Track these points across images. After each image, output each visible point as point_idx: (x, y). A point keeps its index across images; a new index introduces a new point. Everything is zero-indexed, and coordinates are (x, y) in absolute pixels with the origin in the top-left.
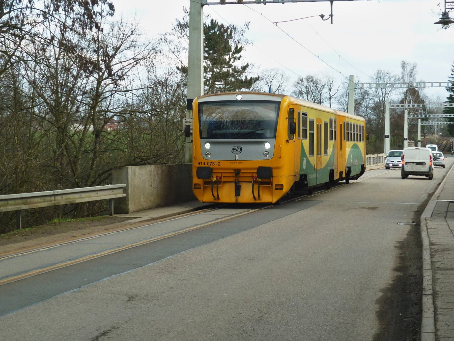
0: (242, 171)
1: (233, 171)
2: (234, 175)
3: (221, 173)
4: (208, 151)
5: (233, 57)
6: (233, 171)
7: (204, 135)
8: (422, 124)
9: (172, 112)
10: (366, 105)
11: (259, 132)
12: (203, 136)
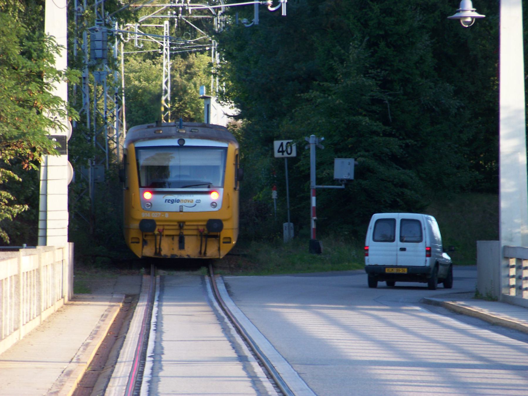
0: (187, 224)
1: (176, 224)
2: (177, 227)
3: (164, 225)
4: (148, 201)
5: (103, 58)
6: (176, 224)
7: (143, 184)
9: (40, 136)
10: (160, 50)
11: (121, 156)
12: (376, 238)
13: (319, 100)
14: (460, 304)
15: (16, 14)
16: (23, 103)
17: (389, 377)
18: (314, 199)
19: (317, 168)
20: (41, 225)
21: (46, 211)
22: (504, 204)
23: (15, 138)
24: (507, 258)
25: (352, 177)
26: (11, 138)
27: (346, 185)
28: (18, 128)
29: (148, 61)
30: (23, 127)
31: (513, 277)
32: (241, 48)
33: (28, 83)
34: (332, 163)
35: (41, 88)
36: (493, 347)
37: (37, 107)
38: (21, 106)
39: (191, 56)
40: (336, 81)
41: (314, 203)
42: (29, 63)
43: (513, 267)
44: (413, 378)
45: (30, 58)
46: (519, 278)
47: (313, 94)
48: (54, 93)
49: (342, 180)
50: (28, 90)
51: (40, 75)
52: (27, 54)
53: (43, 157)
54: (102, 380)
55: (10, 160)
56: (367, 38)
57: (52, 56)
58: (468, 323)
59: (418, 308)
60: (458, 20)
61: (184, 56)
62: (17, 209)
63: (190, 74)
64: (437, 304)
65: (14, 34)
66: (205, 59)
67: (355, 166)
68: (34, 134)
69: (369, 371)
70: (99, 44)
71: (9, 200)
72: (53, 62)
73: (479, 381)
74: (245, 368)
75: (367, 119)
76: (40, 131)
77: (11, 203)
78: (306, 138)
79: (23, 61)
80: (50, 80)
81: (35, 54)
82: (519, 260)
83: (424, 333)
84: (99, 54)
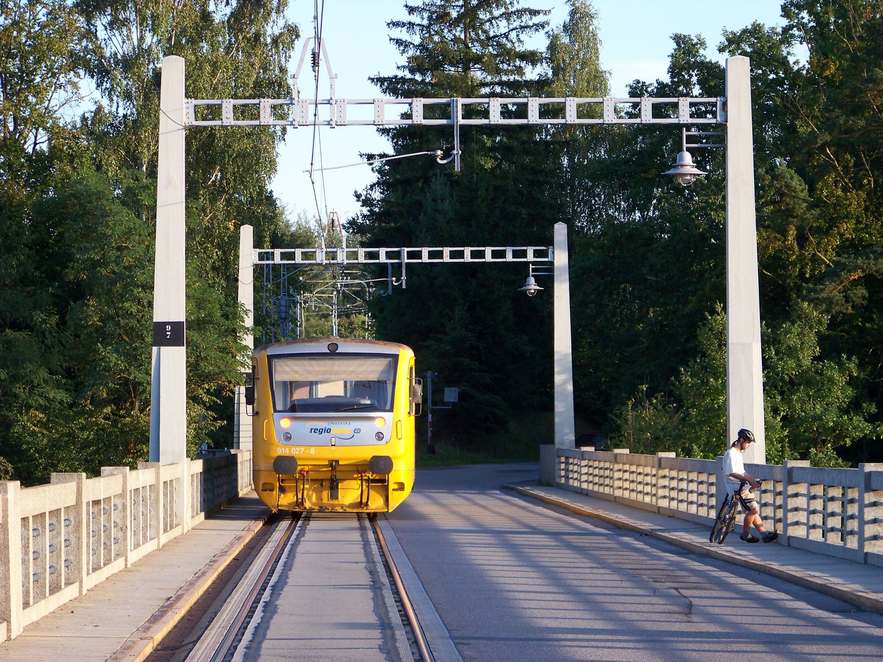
8: (261, 257)
13: (434, 347)
14: (527, 489)
15: (220, 289)
16: (223, 350)
17: (461, 541)
18: (430, 416)
19: (432, 394)
20: (235, 435)
21: (239, 425)
22: (557, 420)
23: (217, 374)
24: (559, 457)
25: (456, 400)
26: (214, 375)
27: (452, 406)
28: (219, 368)
29: (323, 319)
30: (222, 366)
31: (563, 470)
32: (381, 311)
33: (226, 336)
34: (443, 391)
35: (235, 340)
36: (540, 519)
37: (232, 353)
38: (220, 352)
39: (352, 316)
40: (446, 334)
41: (430, 419)
42: (227, 322)
43: (563, 463)
44: (478, 541)
45: (227, 318)
46: (567, 470)
47: (429, 343)
48: (244, 343)
49: (450, 403)
50: (226, 341)
51: (234, 331)
52: (225, 316)
53: (237, 388)
54: (261, 543)
55: (214, 389)
56: (468, 304)
57: (242, 317)
58: (529, 502)
59: (498, 492)
60: (525, 291)
61: (348, 316)
62: (219, 423)
63: (352, 329)
64: (512, 489)
65: (217, 302)
66: (362, 317)
67: (459, 392)
68: (230, 371)
69: (451, 537)
70: (283, 309)
71: (213, 417)
72: (243, 321)
73: (523, 543)
74: (362, 535)
75: (468, 360)
76: (234, 369)
77: (215, 419)
78: (425, 374)
79: (222, 321)
80: (241, 334)
81: (231, 316)
82: (567, 458)
83: (496, 509)
84: (283, 315)
